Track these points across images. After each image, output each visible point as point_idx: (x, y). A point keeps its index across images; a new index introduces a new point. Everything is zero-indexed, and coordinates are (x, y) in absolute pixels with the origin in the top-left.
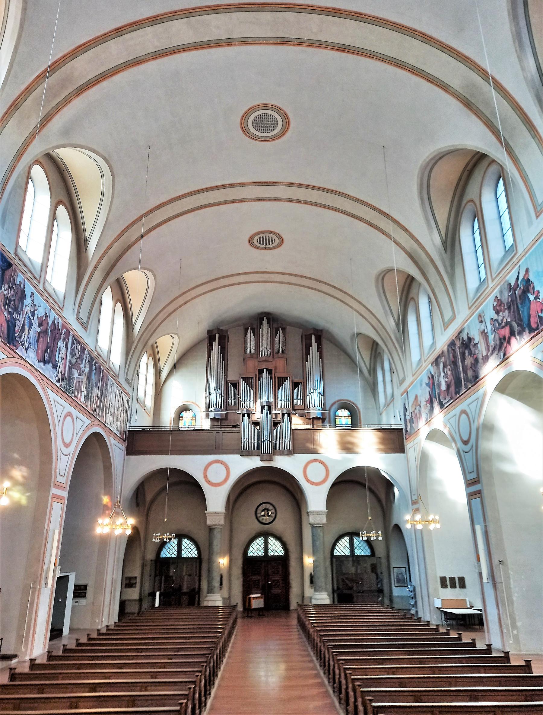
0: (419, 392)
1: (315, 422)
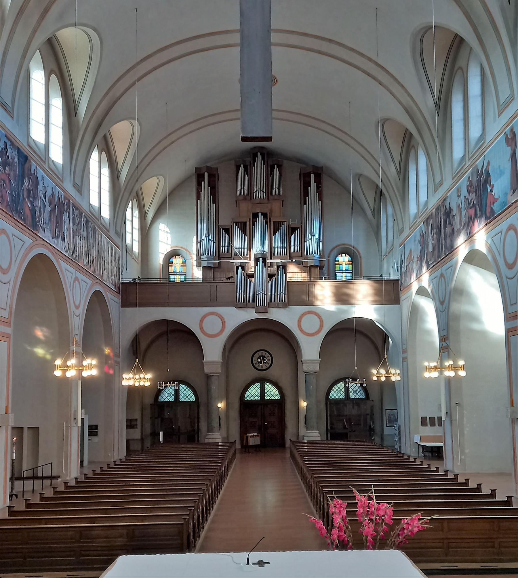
0: (413, 247)
1: (313, 269)
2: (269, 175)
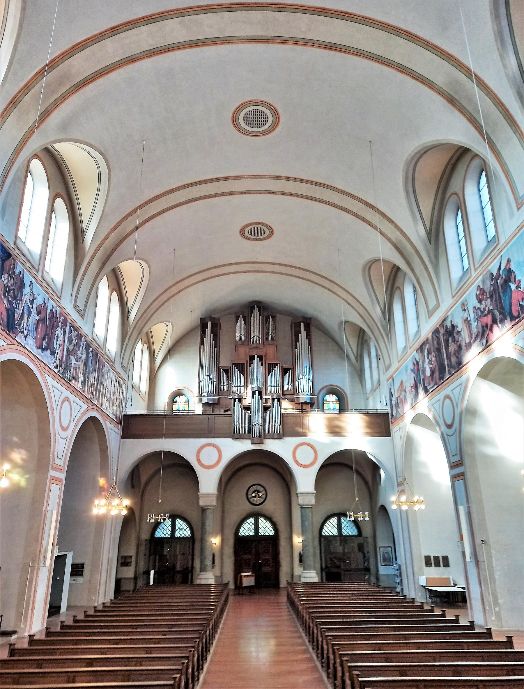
0: (405, 378)
1: (304, 406)
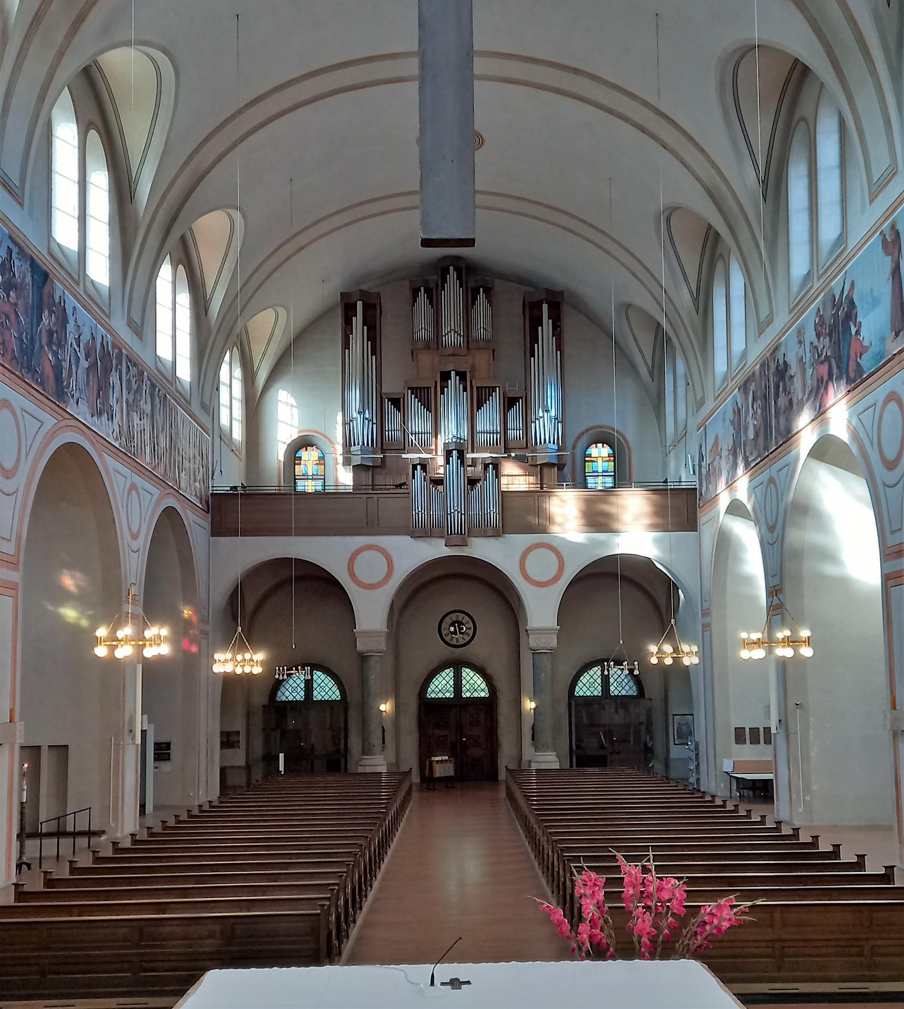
0: (721, 432)
1: (546, 470)
2: (470, 306)
